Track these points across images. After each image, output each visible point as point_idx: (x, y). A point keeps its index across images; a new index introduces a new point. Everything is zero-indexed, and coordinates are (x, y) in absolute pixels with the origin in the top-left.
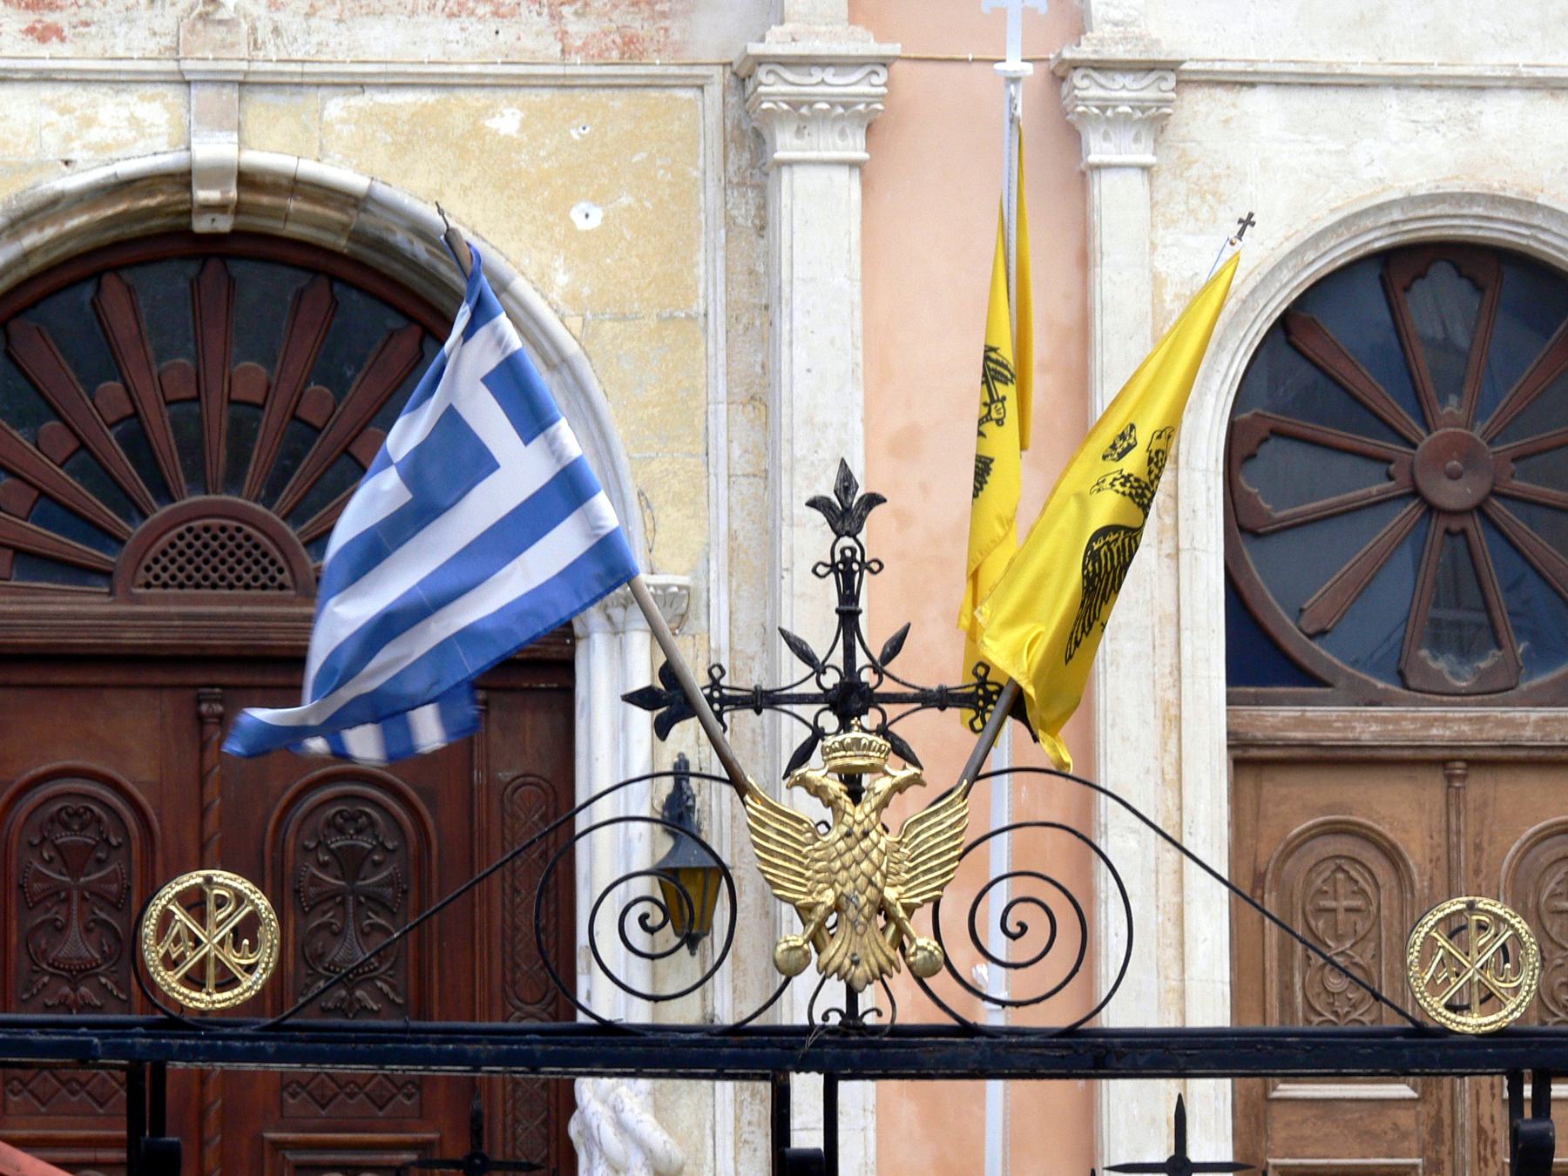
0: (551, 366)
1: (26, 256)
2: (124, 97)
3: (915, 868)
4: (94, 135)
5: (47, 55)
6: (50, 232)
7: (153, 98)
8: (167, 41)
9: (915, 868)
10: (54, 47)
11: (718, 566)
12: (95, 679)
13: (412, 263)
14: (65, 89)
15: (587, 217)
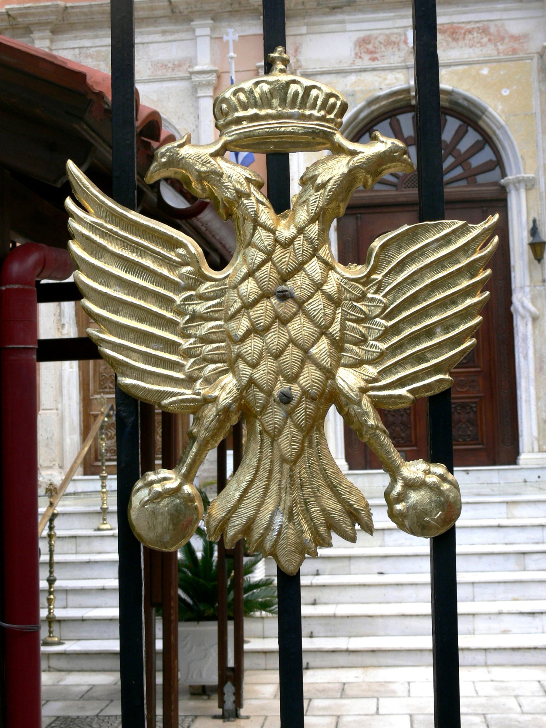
0: (499, 128)
1: (373, 112)
2: (394, 73)
3: (395, 329)
4: (387, 82)
5: (375, 64)
6: (377, 106)
7: (400, 72)
8: (403, 59)
9: (395, 329)
10: (376, 62)
11: (541, 172)
12: (387, 210)
13: (463, 107)
14: (379, 72)
15: (505, 92)
